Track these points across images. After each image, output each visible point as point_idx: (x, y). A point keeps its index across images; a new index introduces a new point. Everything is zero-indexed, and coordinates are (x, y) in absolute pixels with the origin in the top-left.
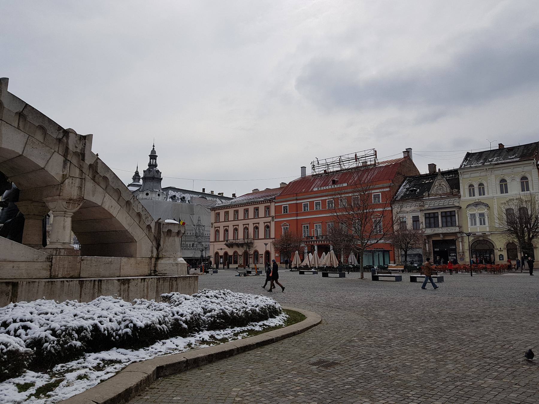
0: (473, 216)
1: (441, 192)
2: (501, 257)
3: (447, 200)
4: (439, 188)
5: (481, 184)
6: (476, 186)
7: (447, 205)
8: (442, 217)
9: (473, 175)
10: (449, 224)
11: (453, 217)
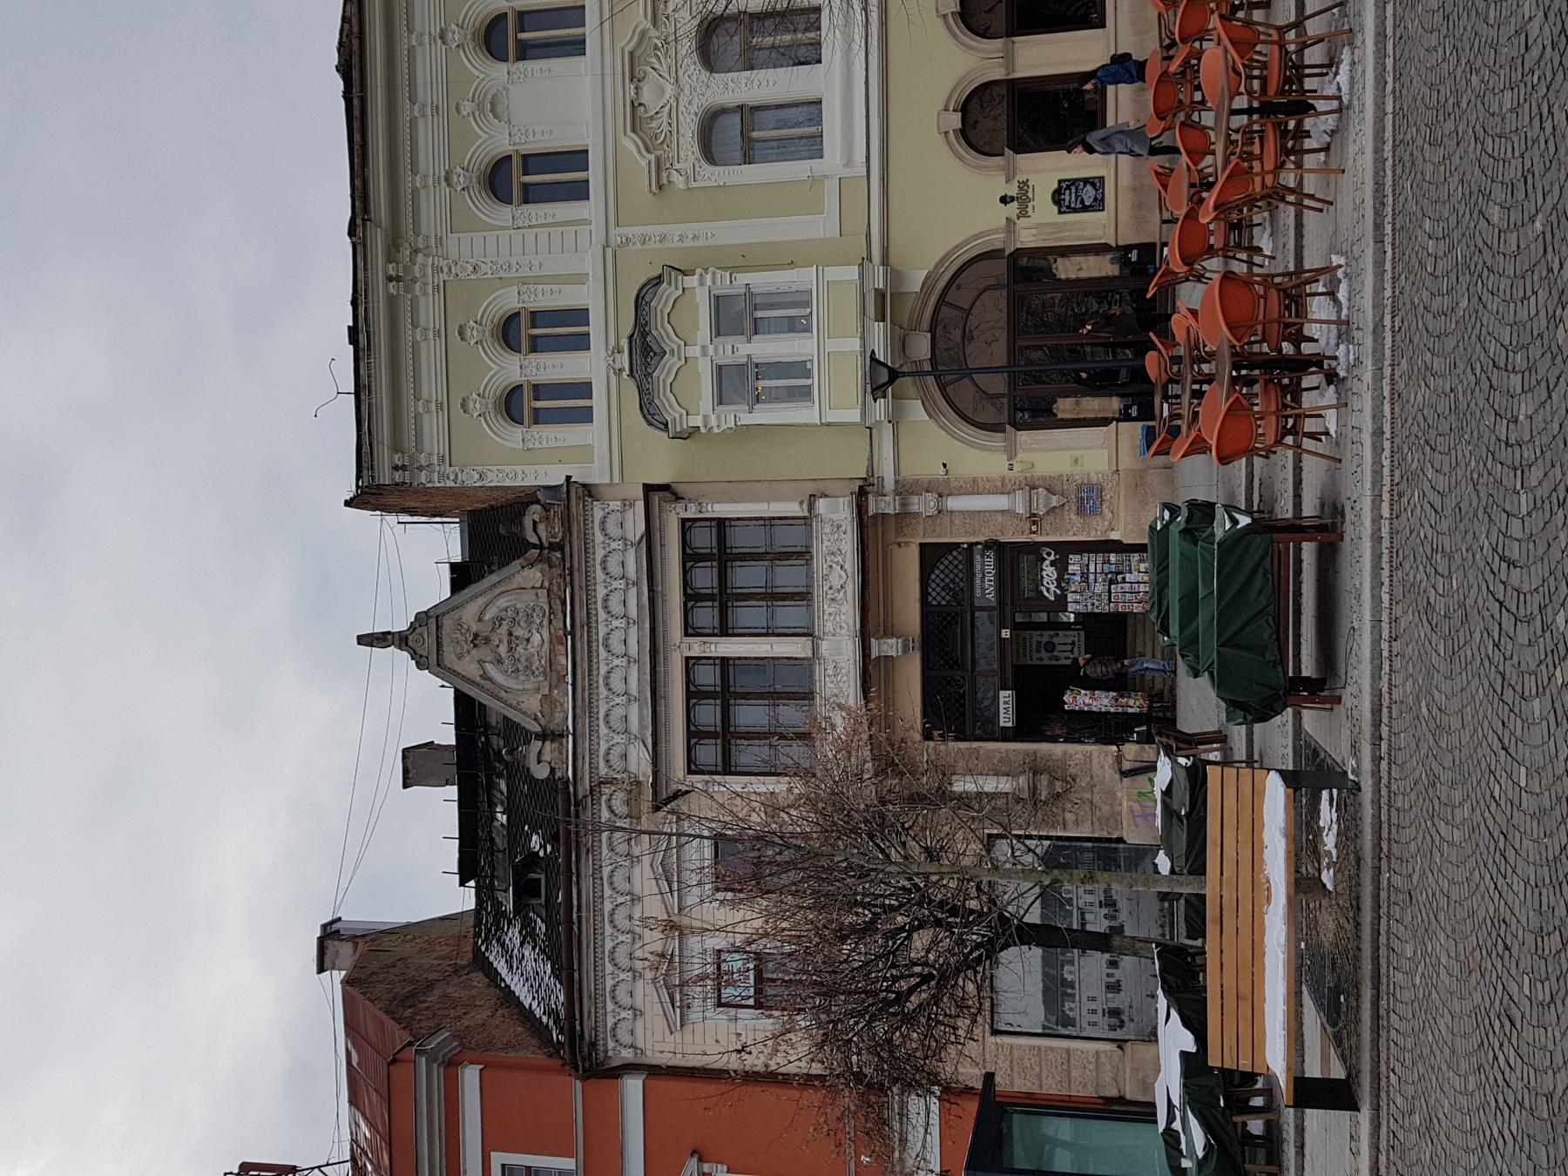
1: (536, 638)
2: (1068, 196)
4: (503, 650)
5: (509, 332)
6: (514, 369)
7: (639, 595)
8: (724, 630)
9: (431, 386)
10: (787, 577)
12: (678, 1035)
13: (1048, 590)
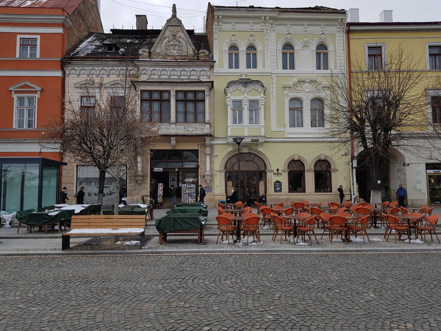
0: (238, 104)
1: (175, 52)
3: (187, 69)
4: (172, 43)
5: (251, 47)
6: (243, 49)
8: (177, 101)
9: (239, 27)
10: (190, 117)
11: (200, 105)
12: (73, 86)
13: (187, 180)
